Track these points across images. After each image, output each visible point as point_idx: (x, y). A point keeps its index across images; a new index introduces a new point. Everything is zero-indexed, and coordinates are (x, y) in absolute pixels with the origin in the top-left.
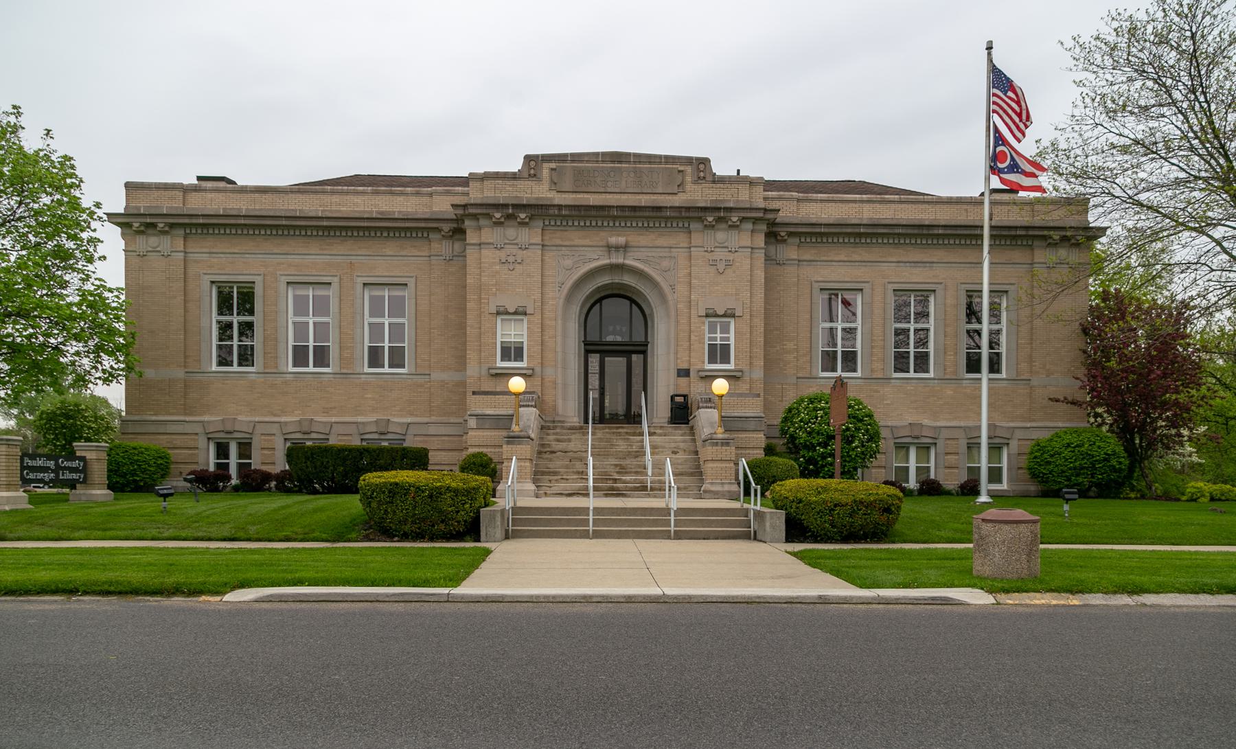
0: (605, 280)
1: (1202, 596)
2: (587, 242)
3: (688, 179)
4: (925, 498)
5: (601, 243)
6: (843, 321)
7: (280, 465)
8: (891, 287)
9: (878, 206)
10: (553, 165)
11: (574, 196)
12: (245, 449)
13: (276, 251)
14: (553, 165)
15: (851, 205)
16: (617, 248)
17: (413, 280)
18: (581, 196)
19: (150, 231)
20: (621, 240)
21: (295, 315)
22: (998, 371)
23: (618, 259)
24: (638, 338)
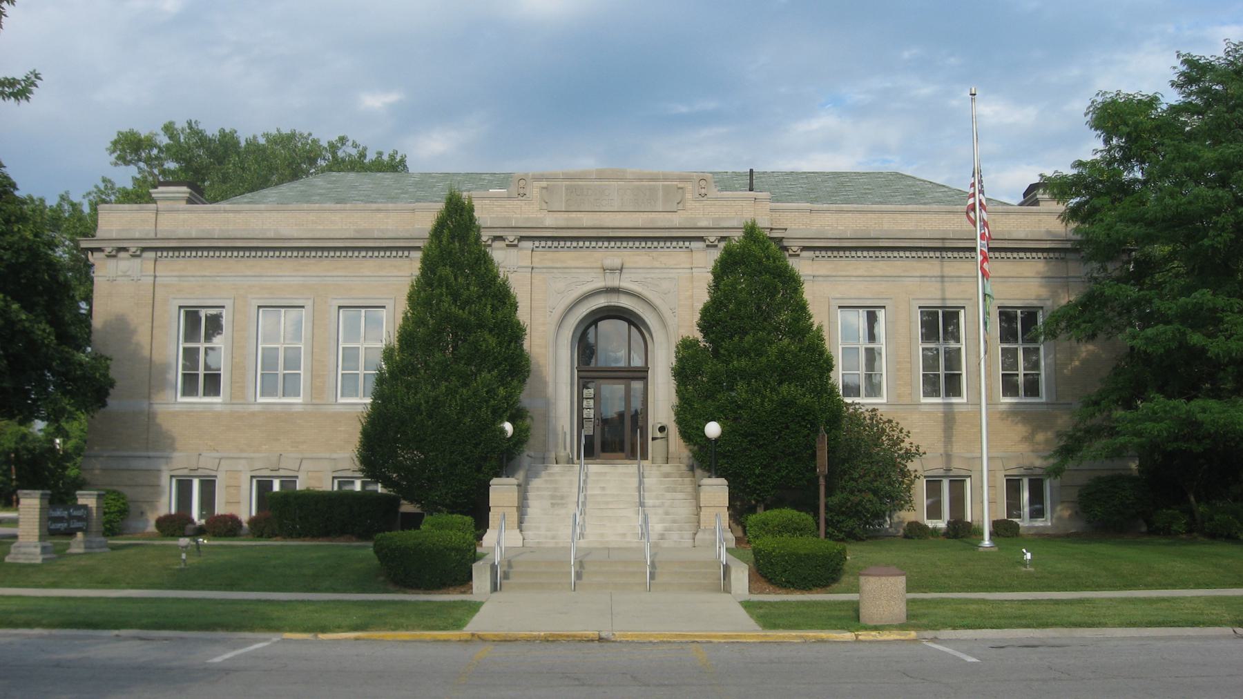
0: (601, 302)
1: (1197, 629)
2: (579, 264)
3: (688, 196)
4: (951, 541)
5: (595, 265)
6: (358, 340)
7: (246, 510)
8: (916, 304)
9: (899, 216)
10: (544, 184)
11: (566, 215)
12: (208, 487)
13: (249, 273)
14: (544, 184)
15: (870, 215)
16: (612, 270)
17: (392, 302)
18: (573, 215)
19: (122, 255)
20: (616, 262)
21: (344, 342)
22: (958, 393)
23: (612, 281)
24: (637, 362)
